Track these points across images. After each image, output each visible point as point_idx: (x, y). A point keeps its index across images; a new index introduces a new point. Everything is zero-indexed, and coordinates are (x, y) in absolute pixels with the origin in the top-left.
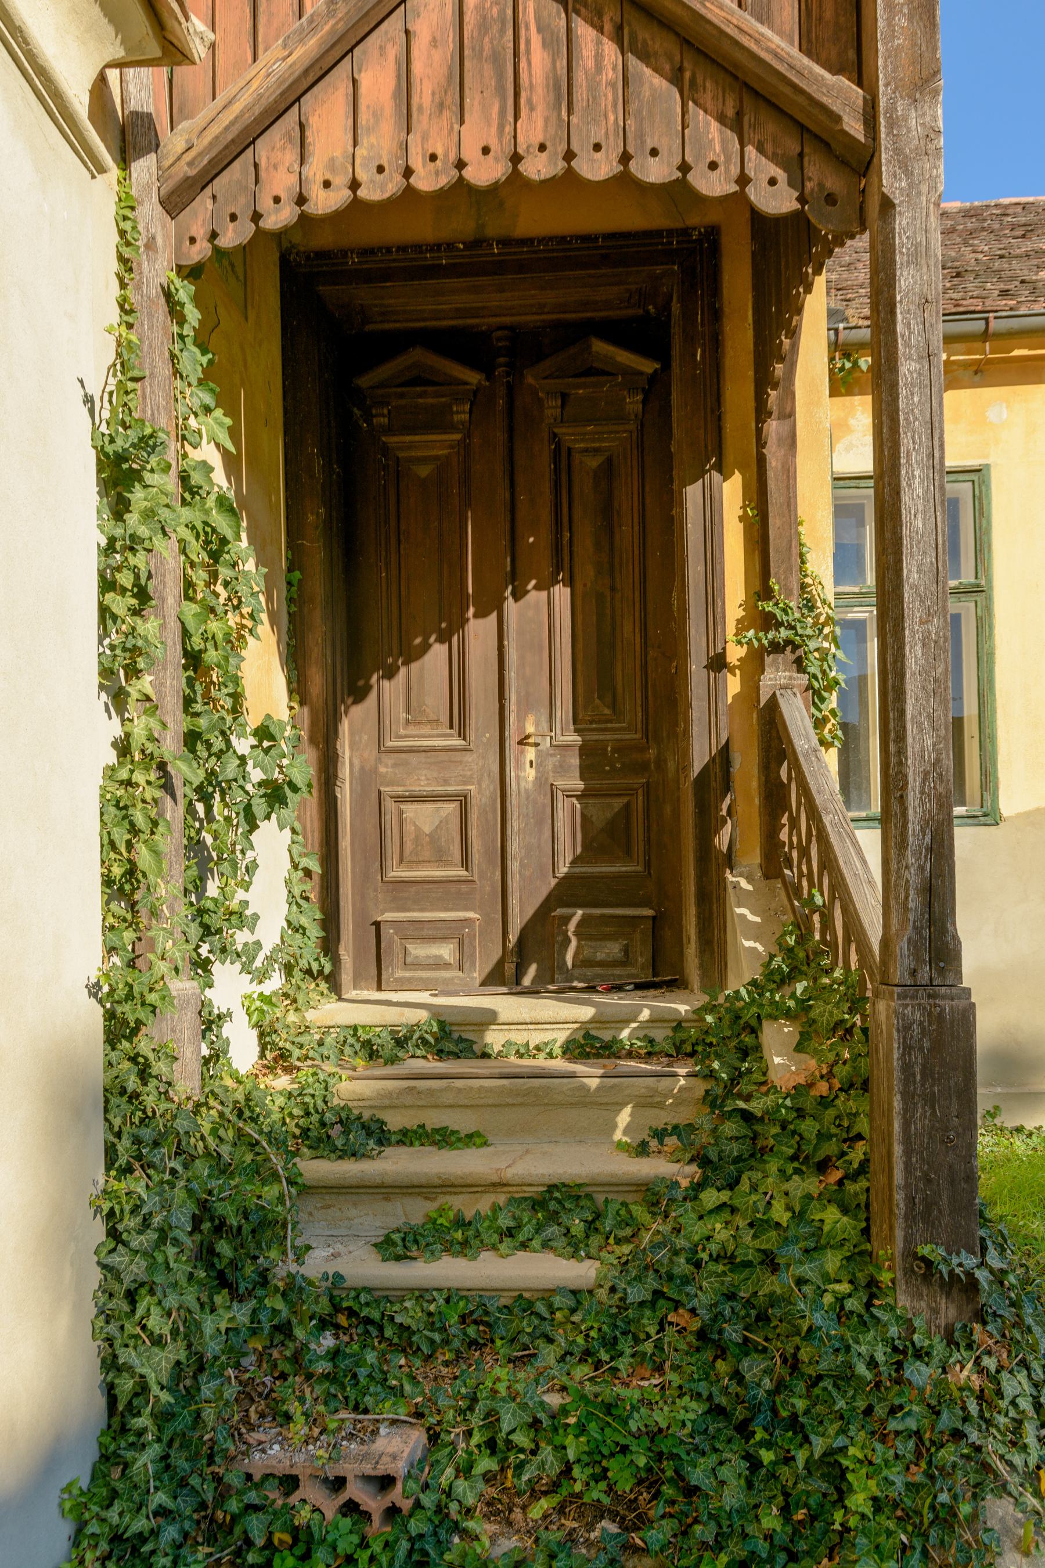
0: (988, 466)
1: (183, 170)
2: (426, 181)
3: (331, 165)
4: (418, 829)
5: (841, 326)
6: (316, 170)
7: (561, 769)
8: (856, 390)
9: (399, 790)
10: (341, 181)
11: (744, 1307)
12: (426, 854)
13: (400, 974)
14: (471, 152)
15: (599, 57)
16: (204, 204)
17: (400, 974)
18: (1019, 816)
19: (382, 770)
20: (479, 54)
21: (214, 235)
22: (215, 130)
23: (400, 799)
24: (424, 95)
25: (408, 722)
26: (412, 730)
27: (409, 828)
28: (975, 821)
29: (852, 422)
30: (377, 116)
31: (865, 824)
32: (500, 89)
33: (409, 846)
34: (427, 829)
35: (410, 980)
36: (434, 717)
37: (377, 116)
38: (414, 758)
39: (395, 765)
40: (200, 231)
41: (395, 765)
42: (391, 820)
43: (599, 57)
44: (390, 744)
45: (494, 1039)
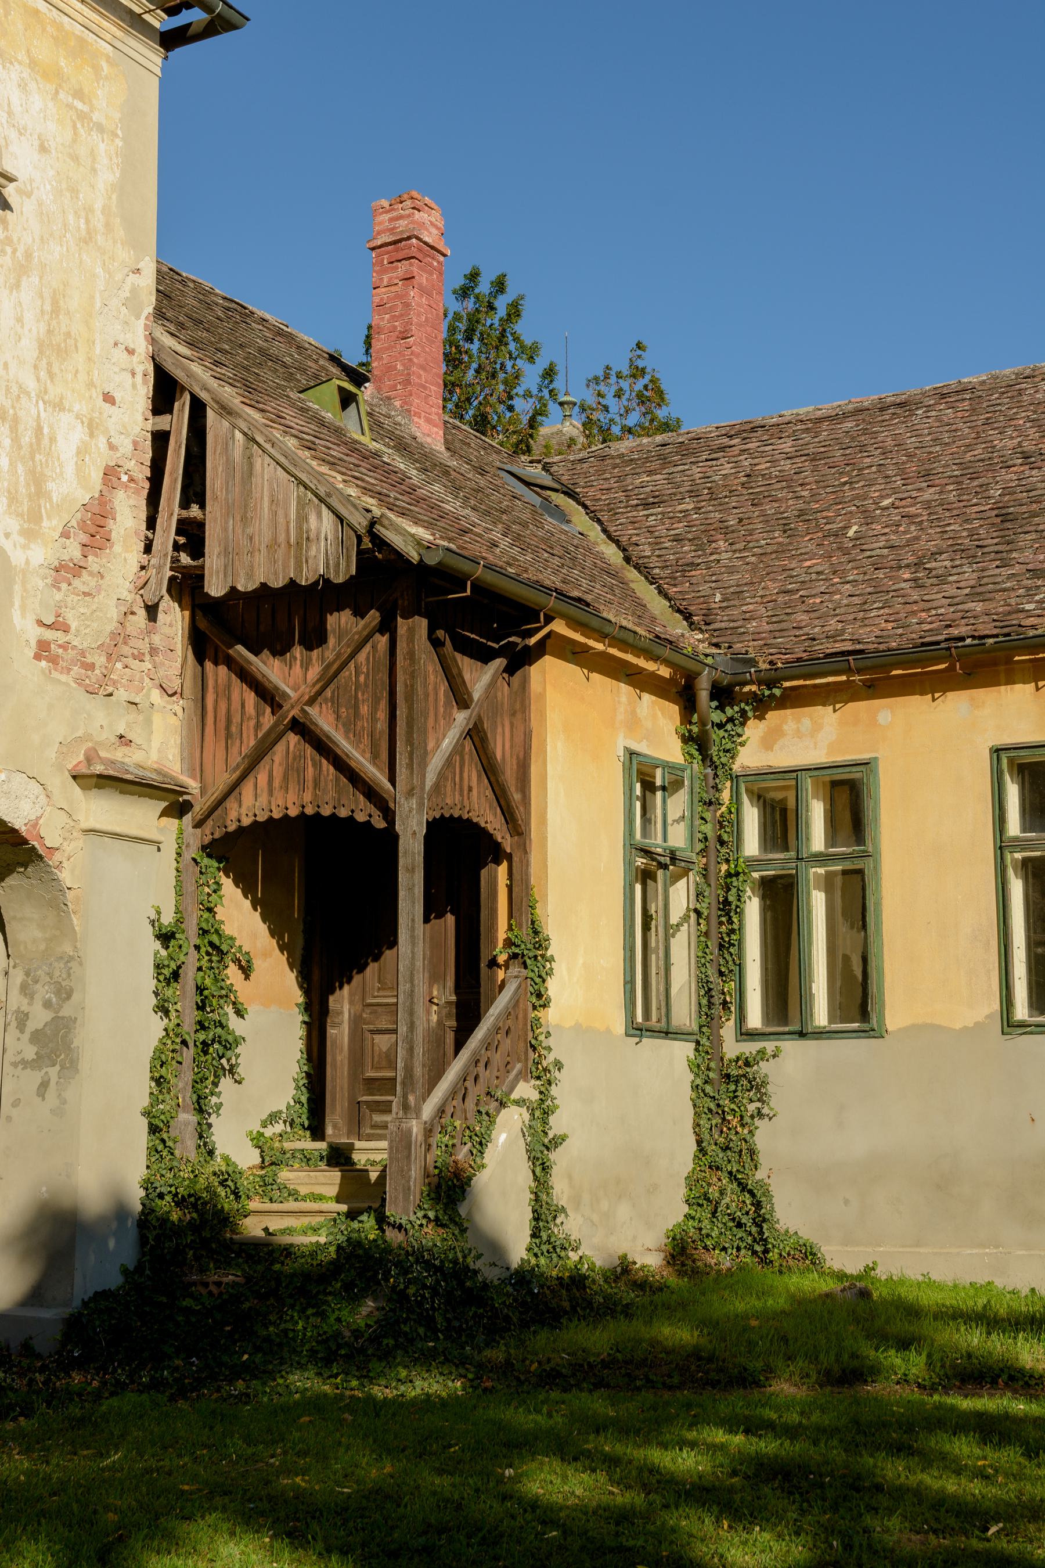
0: (876, 758)
1: (199, 817)
2: (276, 815)
3: (248, 809)
4: (380, 1050)
5: (753, 670)
6: (244, 811)
7: (448, 1016)
8: (788, 704)
9: (371, 1027)
10: (251, 814)
11: (915, 1520)
12: (384, 1063)
13: (369, 1131)
14: (290, 805)
15: (328, 770)
16: (210, 822)
17: (369, 1131)
18: (899, 1030)
19: (365, 1016)
20: (292, 769)
21: (212, 834)
22: (208, 803)
23: (373, 1032)
24: (277, 783)
25: (379, 989)
26: (381, 993)
27: (376, 1048)
28: (866, 1034)
29: (785, 727)
30: (262, 791)
31: (854, 1035)
32: (299, 781)
33: (376, 1059)
34: (384, 1050)
35: (373, 1135)
36: (390, 985)
37: (262, 791)
38: (379, 1009)
39: (371, 1013)
40: (208, 832)
41: (371, 1013)
42: (368, 1043)
43: (328, 770)
44: (369, 1001)
45: (356, 1157)
